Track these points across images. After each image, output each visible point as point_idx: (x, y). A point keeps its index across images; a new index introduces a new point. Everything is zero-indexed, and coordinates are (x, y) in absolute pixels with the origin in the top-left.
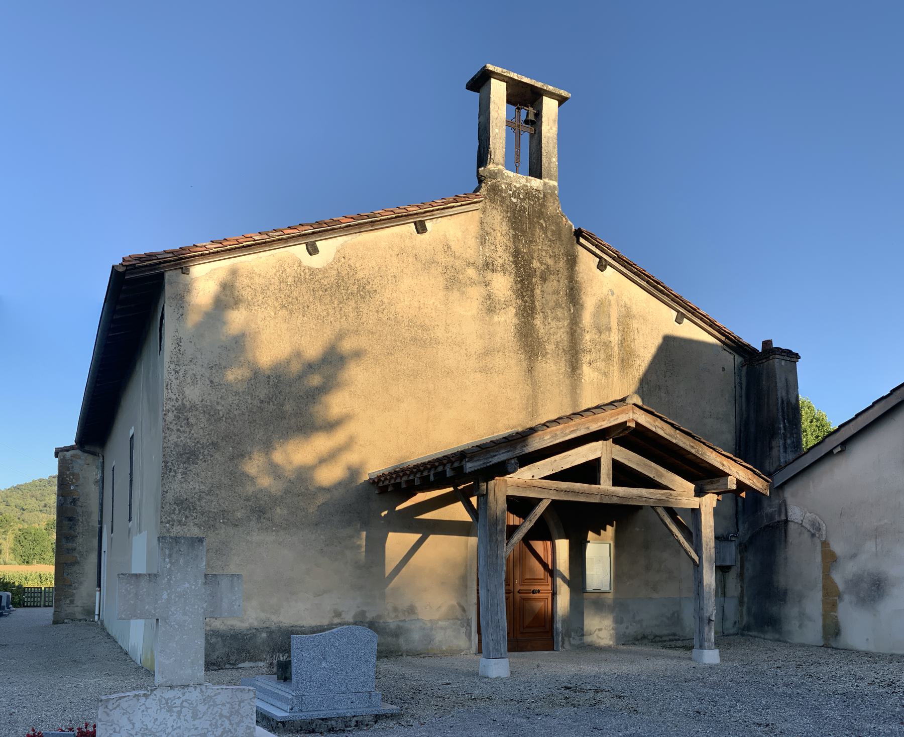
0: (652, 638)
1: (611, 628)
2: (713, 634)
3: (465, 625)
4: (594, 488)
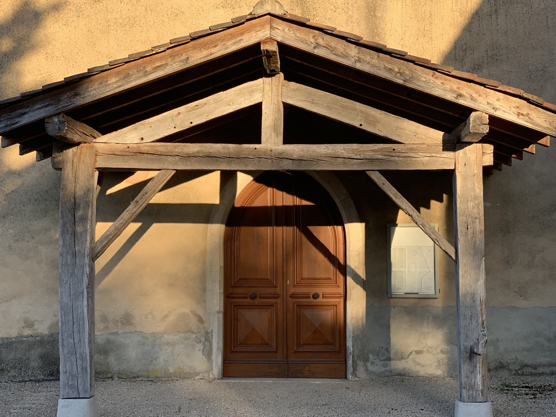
0: (517, 369)
1: (439, 350)
2: (479, 377)
3: (203, 340)
4: (247, 149)
